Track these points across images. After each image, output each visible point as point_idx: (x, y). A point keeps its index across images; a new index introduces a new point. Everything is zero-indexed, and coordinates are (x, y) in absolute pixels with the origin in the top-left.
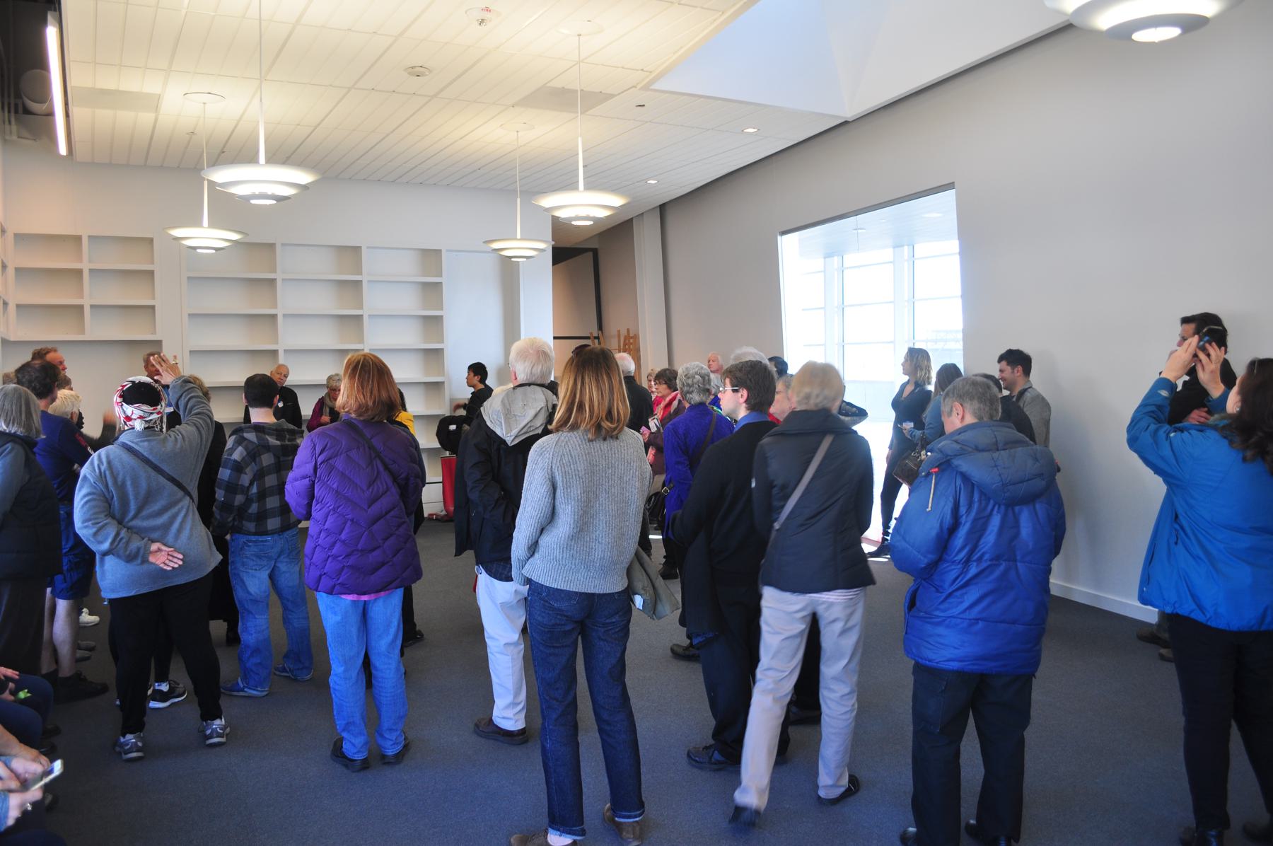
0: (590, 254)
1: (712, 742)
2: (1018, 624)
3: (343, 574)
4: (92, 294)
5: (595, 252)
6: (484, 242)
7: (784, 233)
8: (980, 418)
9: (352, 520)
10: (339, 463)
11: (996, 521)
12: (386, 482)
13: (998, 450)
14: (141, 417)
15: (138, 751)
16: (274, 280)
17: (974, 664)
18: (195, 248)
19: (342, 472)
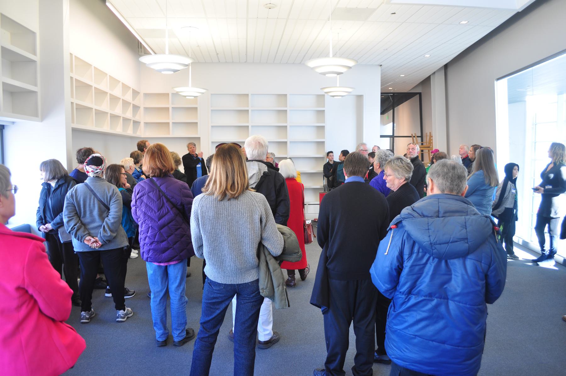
0: (418, 95)
1: (324, 368)
2: (448, 344)
3: (150, 252)
4: (172, 118)
5: (420, 94)
6: (321, 89)
7: (498, 79)
8: (443, 191)
9: (152, 227)
10: (145, 199)
11: (429, 269)
12: (167, 208)
13: (439, 217)
14: (92, 171)
15: (86, 319)
16: (286, 111)
17: (413, 365)
18: (185, 96)
19: (146, 204)
